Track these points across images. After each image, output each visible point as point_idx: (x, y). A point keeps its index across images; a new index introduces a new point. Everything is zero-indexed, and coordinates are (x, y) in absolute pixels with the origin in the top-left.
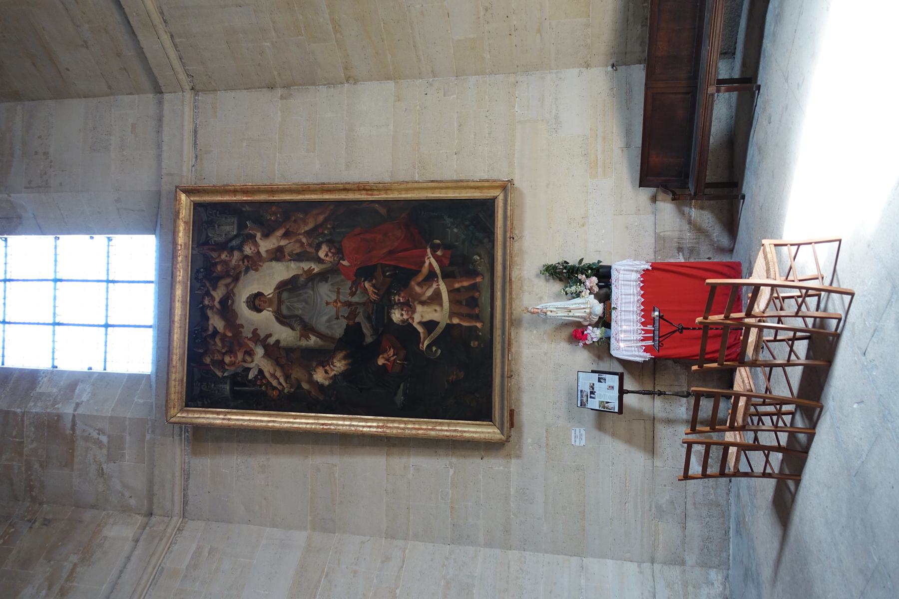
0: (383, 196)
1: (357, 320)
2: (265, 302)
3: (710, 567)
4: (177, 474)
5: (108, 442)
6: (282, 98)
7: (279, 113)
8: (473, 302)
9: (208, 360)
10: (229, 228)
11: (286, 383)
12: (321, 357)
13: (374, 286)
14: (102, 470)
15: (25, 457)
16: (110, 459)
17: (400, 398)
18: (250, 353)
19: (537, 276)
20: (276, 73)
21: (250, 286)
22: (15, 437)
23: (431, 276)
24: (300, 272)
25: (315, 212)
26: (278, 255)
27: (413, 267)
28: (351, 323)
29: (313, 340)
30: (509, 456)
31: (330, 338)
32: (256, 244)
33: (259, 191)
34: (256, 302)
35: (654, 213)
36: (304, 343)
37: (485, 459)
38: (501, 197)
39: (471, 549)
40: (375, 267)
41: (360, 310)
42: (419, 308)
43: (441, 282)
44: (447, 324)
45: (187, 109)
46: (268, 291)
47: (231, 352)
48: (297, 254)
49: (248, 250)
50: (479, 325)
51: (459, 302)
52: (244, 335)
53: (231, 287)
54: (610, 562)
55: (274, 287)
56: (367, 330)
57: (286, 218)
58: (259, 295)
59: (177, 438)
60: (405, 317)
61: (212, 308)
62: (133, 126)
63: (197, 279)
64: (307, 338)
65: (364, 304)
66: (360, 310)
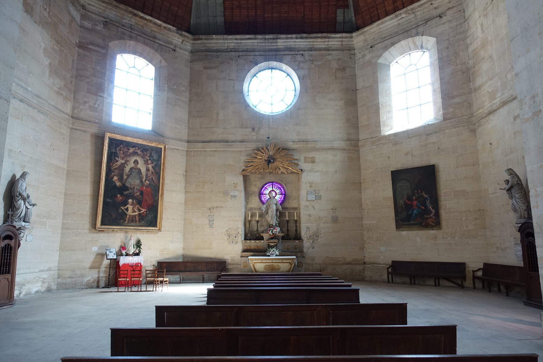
0: (160, 199)
1: (130, 190)
2: (136, 165)
3: (57, 285)
4: (86, 129)
5: (95, 107)
6: (183, 174)
7: (180, 173)
8: (132, 221)
9: (121, 146)
10: (155, 157)
11: (114, 168)
12: (121, 179)
13: (138, 195)
14: (86, 103)
15: (91, 77)
16: (90, 107)
17: (108, 200)
18: (123, 159)
19: (137, 238)
20: (189, 174)
21: (140, 160)
22: (97, 75)
23: (140, 210)
24: (143, 175)
25: (157, 181)
26: (148, 170)
27: (142, 206)
28: (129, 188)
29: (125, 177)
30: (90, 230)
31: (125, 183)
32: (151, 164)
33: (164, 167)
34: (136, 162)
35: (150, 266)
36: (125, 174)
37: (89, 223)
38: (157, 229)
39: (61, 218)
40: (143, 196)
41: (132, 191)
42: (132, 207)
43: (138, 213)
44: (127, 214)
45: (183, 148)
46: (139, 166)
47: (123, 153)
48: (147, 175)
49: (149, 162)
50: (126, 222)
51: (132, 218)
52: (128, 158)
53: (140, 155)
54: (58, 258)
55: (140, 168)
56: (127, 192)
57: (157, 173)
58: (138, 163)
59: (97, 131)
60: (130, 203)
61: (135, 149)
62: (180, 132)
63: (143, 146)
64: (126, 176)
65: (134, 192)
66: (132, 191)
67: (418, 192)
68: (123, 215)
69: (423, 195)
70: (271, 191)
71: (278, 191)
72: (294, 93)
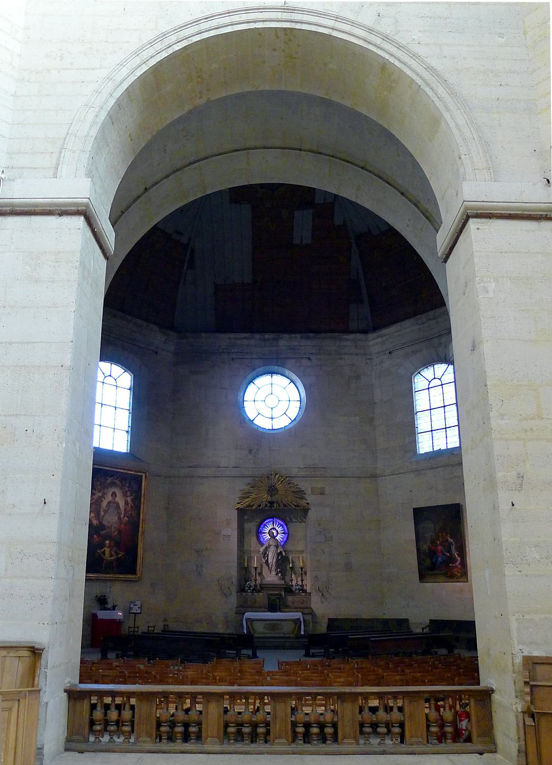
10: (135, 487)
18: (100, 491)
23: (117, 554)
26: (126, 503)
29: (102, 513)
31: (102, 520)
32: (130, 496)
34: (114, 495)
36: (102, 510)
42: (109, 550)
49: (128, 493)
67: (442, 535)
68: (104, 487)
69: (447, 540)
70: (271, 529)
71: (280, 529)
72: (299, 404)
